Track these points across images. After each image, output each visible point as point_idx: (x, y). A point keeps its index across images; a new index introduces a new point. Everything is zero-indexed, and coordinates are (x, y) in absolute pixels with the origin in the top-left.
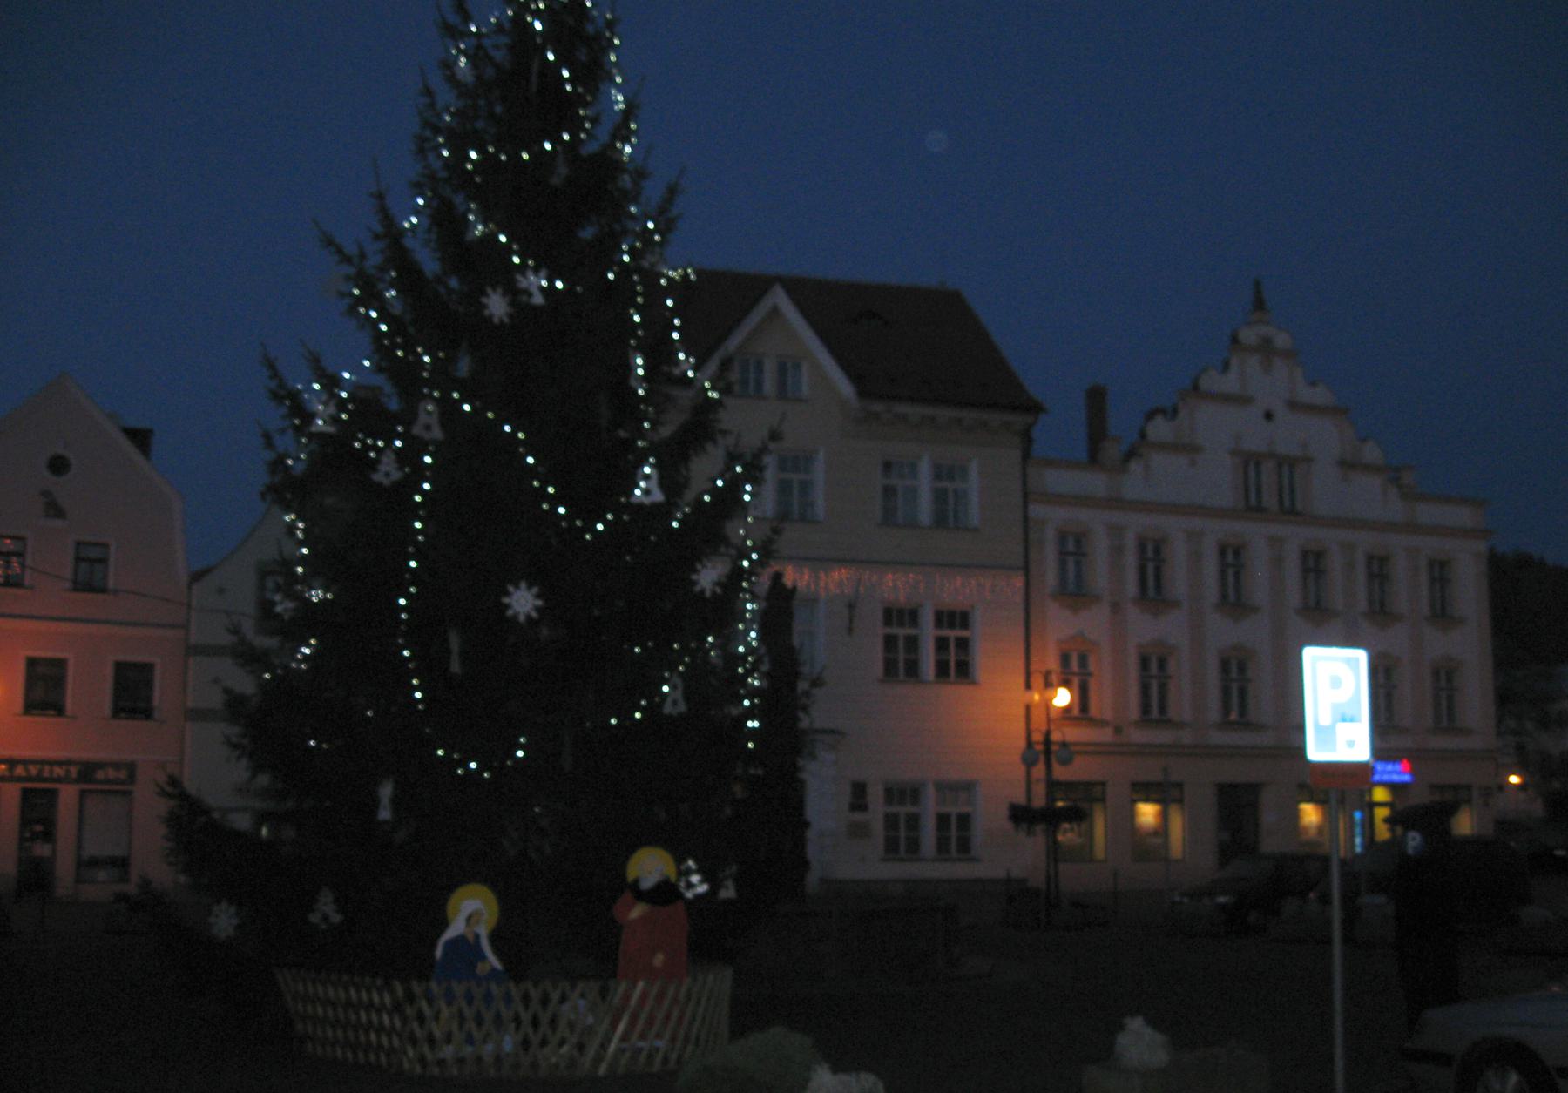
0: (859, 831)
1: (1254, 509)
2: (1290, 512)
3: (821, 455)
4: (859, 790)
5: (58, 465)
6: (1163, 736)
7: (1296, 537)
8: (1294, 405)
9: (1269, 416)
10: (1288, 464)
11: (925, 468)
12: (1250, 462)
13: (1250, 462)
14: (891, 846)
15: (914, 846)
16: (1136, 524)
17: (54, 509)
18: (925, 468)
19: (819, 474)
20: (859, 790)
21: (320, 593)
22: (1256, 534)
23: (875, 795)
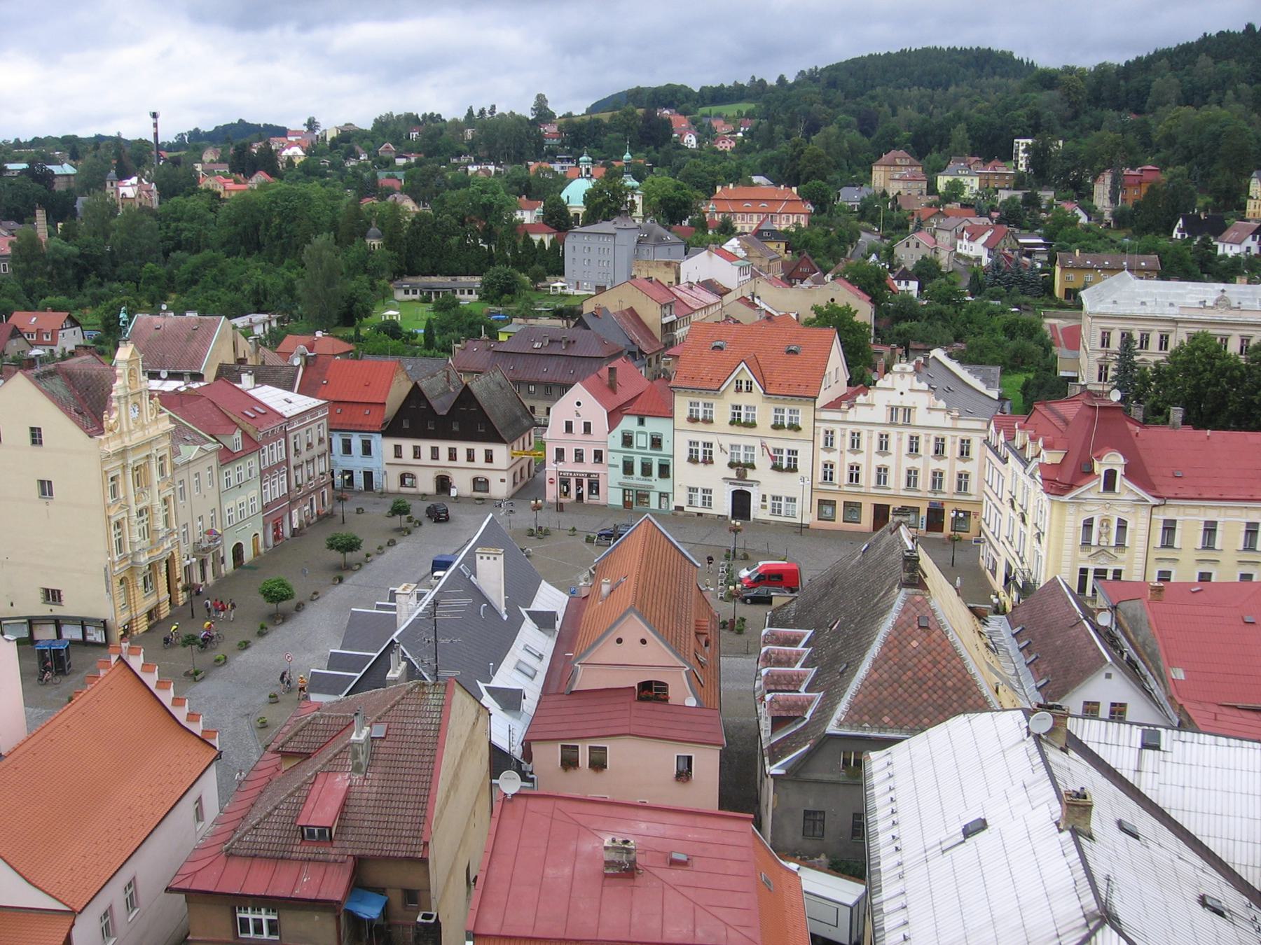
0: (764, 507)
1: (893, 423)
2: (908, 424)
3: (202, 384)
4: (764, 496)
5: (579, 404)
6: (855, 489)
7: (907, 432)
8: (911, 390)
9: (902, 393)
10: (908, 411)
11: (787, 411)
12: (893, 409)
13: (893, 409)
14: (774, 511)
15: (780, 511)
16: (850, 428)
17: (578, 415)
18: (787, 411)
19: (800, 416)
20: (764, 496)
21: (366, 157)
22: (893, 432)
23: (769, 499)
